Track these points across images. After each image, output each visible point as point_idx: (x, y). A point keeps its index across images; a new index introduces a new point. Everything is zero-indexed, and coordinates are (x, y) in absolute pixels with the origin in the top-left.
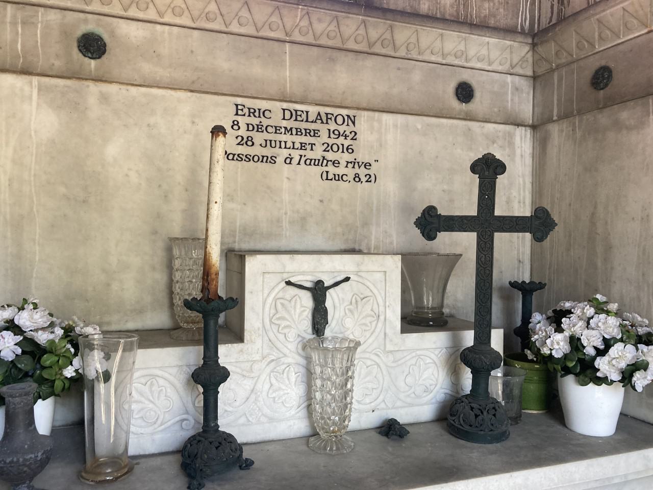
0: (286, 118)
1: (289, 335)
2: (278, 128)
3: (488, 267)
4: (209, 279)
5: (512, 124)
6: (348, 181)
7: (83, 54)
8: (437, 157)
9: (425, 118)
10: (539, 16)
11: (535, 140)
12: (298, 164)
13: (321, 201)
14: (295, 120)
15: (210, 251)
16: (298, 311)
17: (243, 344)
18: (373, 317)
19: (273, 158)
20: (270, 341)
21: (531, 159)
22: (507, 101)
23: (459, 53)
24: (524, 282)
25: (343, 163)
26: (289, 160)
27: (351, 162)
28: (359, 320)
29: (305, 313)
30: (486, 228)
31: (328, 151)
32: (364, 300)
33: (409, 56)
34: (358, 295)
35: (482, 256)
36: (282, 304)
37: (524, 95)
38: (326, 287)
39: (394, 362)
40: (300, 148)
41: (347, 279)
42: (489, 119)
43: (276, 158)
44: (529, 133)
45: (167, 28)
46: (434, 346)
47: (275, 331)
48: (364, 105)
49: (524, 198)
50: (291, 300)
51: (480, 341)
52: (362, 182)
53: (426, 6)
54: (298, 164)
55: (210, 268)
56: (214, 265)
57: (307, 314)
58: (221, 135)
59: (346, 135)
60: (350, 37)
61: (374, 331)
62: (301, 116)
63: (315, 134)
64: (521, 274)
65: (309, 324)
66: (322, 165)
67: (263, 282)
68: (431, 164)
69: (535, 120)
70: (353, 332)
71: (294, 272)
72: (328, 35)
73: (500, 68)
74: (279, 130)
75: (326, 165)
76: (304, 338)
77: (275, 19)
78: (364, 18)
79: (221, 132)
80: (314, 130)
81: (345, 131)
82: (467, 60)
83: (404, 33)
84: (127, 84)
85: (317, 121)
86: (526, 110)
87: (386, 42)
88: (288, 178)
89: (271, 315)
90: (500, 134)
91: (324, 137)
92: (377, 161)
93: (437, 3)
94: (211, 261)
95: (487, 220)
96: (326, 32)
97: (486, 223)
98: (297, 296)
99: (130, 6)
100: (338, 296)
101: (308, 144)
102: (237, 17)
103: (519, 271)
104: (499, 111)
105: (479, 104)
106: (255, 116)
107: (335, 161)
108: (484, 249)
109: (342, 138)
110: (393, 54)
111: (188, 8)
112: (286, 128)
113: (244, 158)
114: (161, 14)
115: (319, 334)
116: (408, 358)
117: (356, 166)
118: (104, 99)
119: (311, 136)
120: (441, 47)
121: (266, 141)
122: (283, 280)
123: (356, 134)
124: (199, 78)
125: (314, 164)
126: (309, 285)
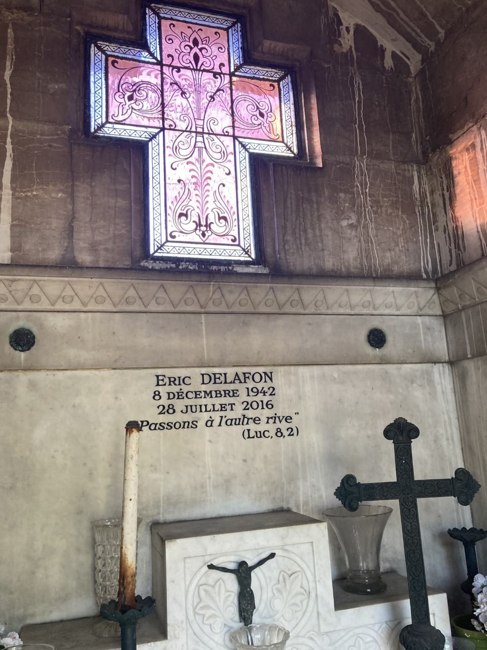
0: (205, 383)
1: (215, 625)
2: (198, 393)
3: (415, 536)
4: (125, 583)
5: (428, 362)
6: (270, 437)
7: (14, 348)
8: (357, 403)
9: (341, 367)
10: (440, 258)
11: (454, 376)
12: (219, 426)
13: (245, 461)
14: (214, 383)
15: (126, 552)
16: (223, 597)
17: (166, 641)
18: (303, 594)
19: (194, 423)
20: (195, 634)
21: (454, 394)
22: (421, 342)
23: (366, 304)
24: (464, 529)
25: (264, 420)
26: (210, 423)
27: (272, 418)
28: (288, 600)
29: (231, 599)
30: (408, 494)
31: (248, 409)
32: (292, 577)
33: (319, 312)
34: (285, 572)
35: (408, 525)
36: (206, 591)
37: (436, 333)
38: (250, 567)
39: (331, 644)
40: (220, 409)
41: (272, 556)
42: (404, 360)
43: (197, 422)
44: (447, 369)
45: (90, 314)
46: (372, 622)
47: (200, 622)
48: (280, 362)
49: (452, 434)
50: (214, 585)
51: (418, 620)
52: (284, 436)
53: (331, 263)
54: (219, 426)
55: (126, 571)
56: (129, 567)
57: (234, 599)
58: (135, 430)
59: (264, 391)
60: (261, 302)
61: (305, 611)
62: (219, 378)
63: (234, 393)
64: (461, 517)
65: (236, 611)
66: (243, 424)
67: (185, 567)
68: (352, 411)
69: (451, 356)
70: (283, 615)
71: (216, 554)
72: (239, 303)
73: (409, 312)
74: (199, 395)
75: (247, 424)
76: (231, 628)
77: (190, 295)
78: (272, 285)
79: (135, 428)
80: (233, 391)
81: (263, 388)
82: (375, 308)
83: (311, 293)
84: (54, 370)
85: (236, 381)
86: (440, 345)
87: (295, 303)
88: (210, 441)
89: (195, 604)
90: (418, 374)
91: (243, 396)
92: (298, 413)
93: (341, 258)
94: (127, 563)
95: (407, 486)
96: (238, 300)
97: (408, 489)
98: (221, 580)
99: (56, 301)
100: (264, 574)
101: (227, 405)
102: (155, 298)
103: (458, 513)
104: (414, 351)
105: (392, 347)
106: (175, 384)
107: (255, 418)
108: (409, 516)
109: (261, 395)
110: (302, 311)
111: (109, 296)
112: (205, 392)
113: (166, 426)
114: (84, 304)
115: (247, 623)
116: (345, 638)
117: (277, 419)
118: (33, 386)
119: (230, 396)
120: (348, 301)
121: (187, 407)
122: (205, 564)
123: (274, 389)
124: (120, 357)
125: (235, 424)
126: (232, 566)
